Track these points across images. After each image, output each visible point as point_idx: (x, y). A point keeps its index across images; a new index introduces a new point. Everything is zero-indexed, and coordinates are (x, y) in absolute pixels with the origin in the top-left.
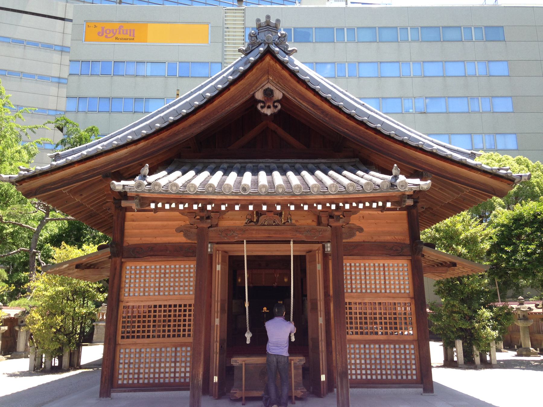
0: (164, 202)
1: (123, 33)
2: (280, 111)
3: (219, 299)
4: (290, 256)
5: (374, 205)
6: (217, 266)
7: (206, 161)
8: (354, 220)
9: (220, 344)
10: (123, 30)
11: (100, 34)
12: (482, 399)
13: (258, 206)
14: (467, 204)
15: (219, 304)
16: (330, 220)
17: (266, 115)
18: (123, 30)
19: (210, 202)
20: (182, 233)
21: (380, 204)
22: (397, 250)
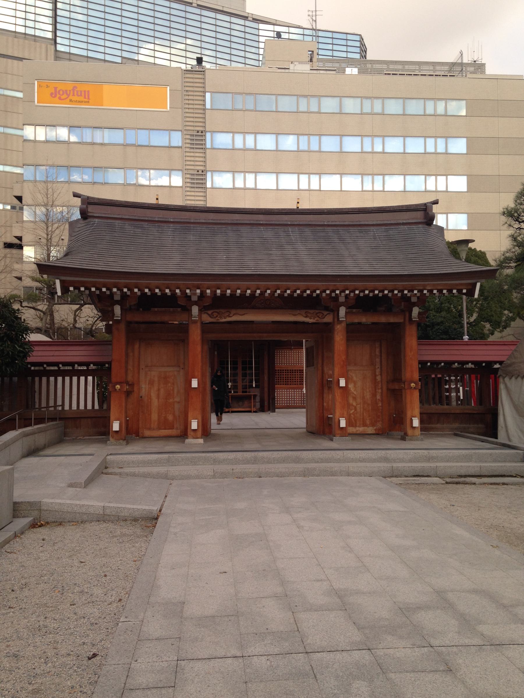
1: (78, 95)
11: (53, 95)
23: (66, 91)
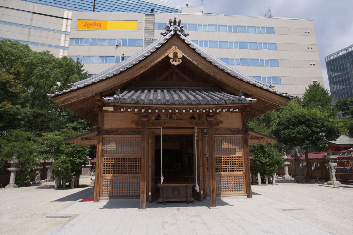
0: (126, 108)
2: (181, 63)
3: (151, 156)
4: (161, 135)
5: (224, 110)
6: (150, 140)
7: (144, 87)
8: (220, 118)
9: (152, 177)
10: (96, 24)
12: (123, 209)
13: (146, 111)
14: (267, 110)
15: (151, 158)
16: (208, 117)
17: (175, 65)
18: (96, 24)
19: (150, 108)
20: (134, 123)
21: (220, 110)
22: (236, 132)
23: (91, 24)
